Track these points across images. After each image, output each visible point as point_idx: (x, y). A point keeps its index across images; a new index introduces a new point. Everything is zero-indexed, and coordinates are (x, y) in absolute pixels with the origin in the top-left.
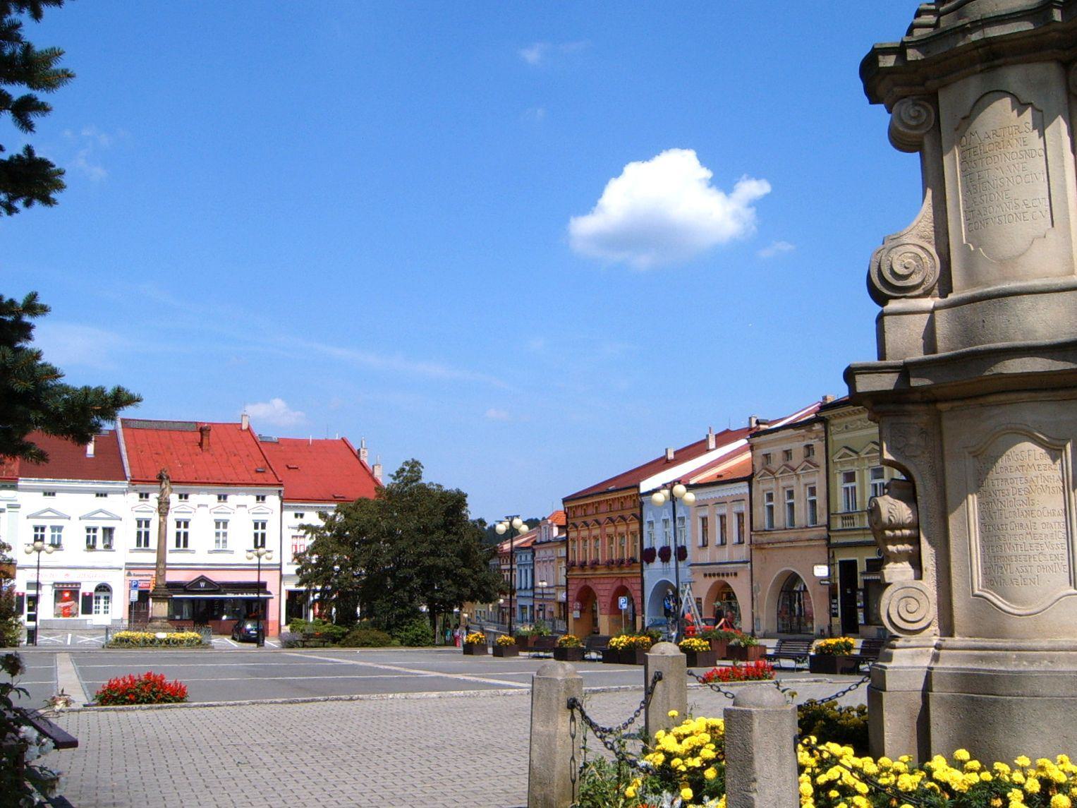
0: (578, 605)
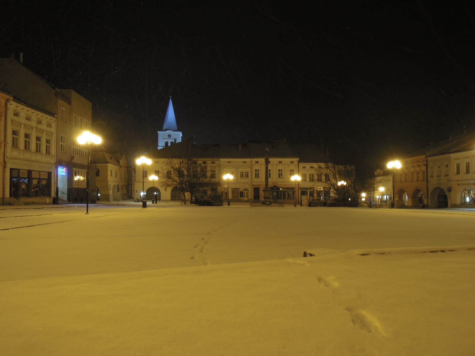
0: (398, 196)
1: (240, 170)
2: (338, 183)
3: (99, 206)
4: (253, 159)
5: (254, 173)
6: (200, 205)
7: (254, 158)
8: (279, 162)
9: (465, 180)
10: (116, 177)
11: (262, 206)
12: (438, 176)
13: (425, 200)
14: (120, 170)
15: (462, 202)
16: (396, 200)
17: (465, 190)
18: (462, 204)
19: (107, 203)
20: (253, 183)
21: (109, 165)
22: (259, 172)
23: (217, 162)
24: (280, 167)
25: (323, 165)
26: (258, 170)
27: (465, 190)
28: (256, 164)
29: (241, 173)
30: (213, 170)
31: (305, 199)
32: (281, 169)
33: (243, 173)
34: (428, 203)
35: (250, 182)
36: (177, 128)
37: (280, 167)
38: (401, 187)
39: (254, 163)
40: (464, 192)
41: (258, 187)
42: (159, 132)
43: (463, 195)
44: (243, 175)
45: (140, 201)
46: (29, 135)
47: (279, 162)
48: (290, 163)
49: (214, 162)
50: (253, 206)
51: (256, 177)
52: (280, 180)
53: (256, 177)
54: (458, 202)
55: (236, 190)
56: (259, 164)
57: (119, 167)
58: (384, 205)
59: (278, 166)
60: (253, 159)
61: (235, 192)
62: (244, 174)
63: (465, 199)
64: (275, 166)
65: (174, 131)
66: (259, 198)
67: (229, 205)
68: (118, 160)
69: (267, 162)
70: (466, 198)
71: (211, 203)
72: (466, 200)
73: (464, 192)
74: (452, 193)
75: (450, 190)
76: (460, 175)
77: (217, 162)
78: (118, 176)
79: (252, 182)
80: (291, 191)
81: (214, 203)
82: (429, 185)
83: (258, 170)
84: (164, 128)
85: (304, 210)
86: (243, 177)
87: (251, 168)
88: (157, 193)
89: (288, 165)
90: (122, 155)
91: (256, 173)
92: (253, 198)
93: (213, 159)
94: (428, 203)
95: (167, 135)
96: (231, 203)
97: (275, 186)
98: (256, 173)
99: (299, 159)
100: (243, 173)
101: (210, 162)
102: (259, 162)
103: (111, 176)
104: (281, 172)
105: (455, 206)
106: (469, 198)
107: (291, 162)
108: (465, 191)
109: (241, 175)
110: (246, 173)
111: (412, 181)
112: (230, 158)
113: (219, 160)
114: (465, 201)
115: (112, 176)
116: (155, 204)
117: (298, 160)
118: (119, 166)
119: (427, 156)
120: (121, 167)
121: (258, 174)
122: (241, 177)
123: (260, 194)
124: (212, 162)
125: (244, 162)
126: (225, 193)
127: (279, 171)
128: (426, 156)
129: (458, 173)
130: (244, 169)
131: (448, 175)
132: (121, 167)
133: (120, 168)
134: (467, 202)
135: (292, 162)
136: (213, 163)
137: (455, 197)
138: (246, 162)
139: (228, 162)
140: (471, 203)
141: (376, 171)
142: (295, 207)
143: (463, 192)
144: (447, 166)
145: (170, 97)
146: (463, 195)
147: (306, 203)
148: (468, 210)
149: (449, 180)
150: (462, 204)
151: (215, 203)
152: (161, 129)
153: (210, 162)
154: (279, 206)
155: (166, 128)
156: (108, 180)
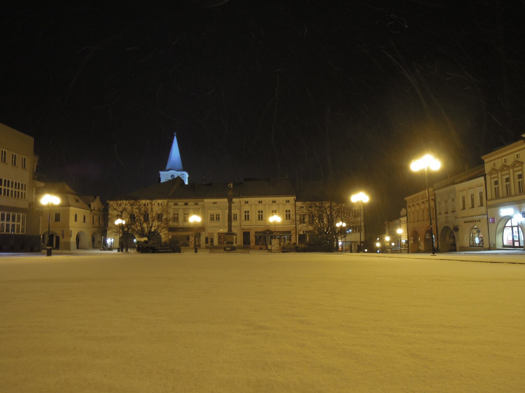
0: (412, 238)
1: (210, 212)
2: (336, 223)
3: (22, 255)
4: (241, 199)
5: (243, 215)
6: (142, 252)
7: (243, 198)
8: (246, 202)
9: (472, 216)
10: (84, 222)
11: (223, 253)
12: (445, 213)
13: (421, 242)
14: (91, 214)
15: (471, 243)
16: (411, 244)
17: (473, 228)
18: (471, 246)
19: (68, 252)
20: (242, 227)
21: (71, 208)
22: (250, 214)
23: (200, 203)
24: (260, 208)
25: (301, 204)
26: (248, 212)
27: (473, 228)
28: (273, 204)
29: (211, 215)
30: (176, 213)
31: (275, 244)
32: (248, 210)
33: (213, 215)
34: (438, 246)
35: (238, 225)
36: (181, 168)
37: (260, 208)
38: (414, 228)
39: (243, 203)
40: (472, 232)
41: (248, 231)
42: (161, 173)
43: (471, 235)
44: (213, 217)
45: (107, 250)
46: (34, 179)
47: (273, 202)
48: (285, 202)
49: (197, 204)
50: (215, 253)
51: (260, 219)
52: (261, 222)
53: (245, 219)
54: (467, 244)
55: (223, 235)
56: (263, 205)
57: (90, 211)
58: (403, 249)
59: (284, 206)
60: (241, 199)
61: (222, 237)
62: (214, 216)
63: (474, 240)
64: (253, 206)
65: (178, 171)
66: (249, 244)
67: (196, 252)
68: (90, 203)
69: (230, 202)
70: (475, 238)
71: (157, 250)
72: (475, 240)
73: (472, 232)
74: (460, 232)
75: (456, 229)
76: (466, 209)
77: (200, 203)
78: (87, 220)
79: (241, 226)
80: (269, 236)
81: (161, 250)
82: (438, 225)
83: (248, 212)
84: (168, 168)
85: (203, 255)
86: (213, 220)
87: (240, 210)
88: (390, 242)
89: (270, 205)
90: (95, 197)
91: (260, 215)
92: (242, 244)
93: (196, 200)
94: (438, 246)
95: (170, 176)
96: (198, 250)
97: (268, 230)
98: (245, 215)
99: (295, 197)
100: (213, 215)
101: (193, 203)
102: (276, 202)
103: (76, 220)
104: (289, 213)
105: (463, 249)
106: (479, 238)
107: (273, 202)
108: (473, 230)
109: (211, 217)
110: (217, 215)
111: (423, 220)
112: (218, 198)
113: (203, 201)
114: (474, 242)
115: (86, 221)
116: (120, 252)
117: (294, 198)
118: (89, 210)
119: (434, 189)
120: (92, 211)
121: (248, 215)
122: (211, 220)
123: (251, 240)
124: (195, 203)
125: (215, 203)
126: (210, 238)
127: (259, 212)
128: (433, 189)
129: (464, 208)
130: (214, 211)
131: (455, 211)
132: (92, 211)
133: (91, 212)
134: (476, 244)
135: (288, 201)
136: (176, 204)
137: (463, 239)
138: (217, 203)
139: (213, 203)
140: (481, 245)
141: (401, 210)
142: (196, 254)
143: (471, 232)
144: (453, 200)
145: (175, 133)
146: (471, 235)
147: (277, 248)
148: (465, 254)
149: (456, 218)
150: (471, 246)
151: (162, 249)
152: (164, 169)
153: (193, 203)
154: (243, 252)
155: (170, 168)
156: (70, 226)
